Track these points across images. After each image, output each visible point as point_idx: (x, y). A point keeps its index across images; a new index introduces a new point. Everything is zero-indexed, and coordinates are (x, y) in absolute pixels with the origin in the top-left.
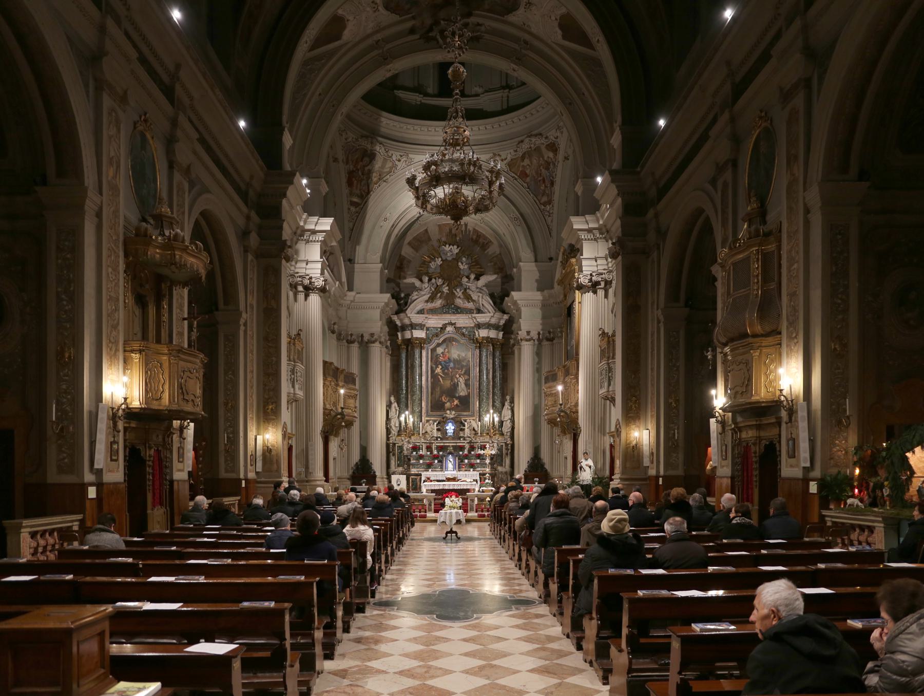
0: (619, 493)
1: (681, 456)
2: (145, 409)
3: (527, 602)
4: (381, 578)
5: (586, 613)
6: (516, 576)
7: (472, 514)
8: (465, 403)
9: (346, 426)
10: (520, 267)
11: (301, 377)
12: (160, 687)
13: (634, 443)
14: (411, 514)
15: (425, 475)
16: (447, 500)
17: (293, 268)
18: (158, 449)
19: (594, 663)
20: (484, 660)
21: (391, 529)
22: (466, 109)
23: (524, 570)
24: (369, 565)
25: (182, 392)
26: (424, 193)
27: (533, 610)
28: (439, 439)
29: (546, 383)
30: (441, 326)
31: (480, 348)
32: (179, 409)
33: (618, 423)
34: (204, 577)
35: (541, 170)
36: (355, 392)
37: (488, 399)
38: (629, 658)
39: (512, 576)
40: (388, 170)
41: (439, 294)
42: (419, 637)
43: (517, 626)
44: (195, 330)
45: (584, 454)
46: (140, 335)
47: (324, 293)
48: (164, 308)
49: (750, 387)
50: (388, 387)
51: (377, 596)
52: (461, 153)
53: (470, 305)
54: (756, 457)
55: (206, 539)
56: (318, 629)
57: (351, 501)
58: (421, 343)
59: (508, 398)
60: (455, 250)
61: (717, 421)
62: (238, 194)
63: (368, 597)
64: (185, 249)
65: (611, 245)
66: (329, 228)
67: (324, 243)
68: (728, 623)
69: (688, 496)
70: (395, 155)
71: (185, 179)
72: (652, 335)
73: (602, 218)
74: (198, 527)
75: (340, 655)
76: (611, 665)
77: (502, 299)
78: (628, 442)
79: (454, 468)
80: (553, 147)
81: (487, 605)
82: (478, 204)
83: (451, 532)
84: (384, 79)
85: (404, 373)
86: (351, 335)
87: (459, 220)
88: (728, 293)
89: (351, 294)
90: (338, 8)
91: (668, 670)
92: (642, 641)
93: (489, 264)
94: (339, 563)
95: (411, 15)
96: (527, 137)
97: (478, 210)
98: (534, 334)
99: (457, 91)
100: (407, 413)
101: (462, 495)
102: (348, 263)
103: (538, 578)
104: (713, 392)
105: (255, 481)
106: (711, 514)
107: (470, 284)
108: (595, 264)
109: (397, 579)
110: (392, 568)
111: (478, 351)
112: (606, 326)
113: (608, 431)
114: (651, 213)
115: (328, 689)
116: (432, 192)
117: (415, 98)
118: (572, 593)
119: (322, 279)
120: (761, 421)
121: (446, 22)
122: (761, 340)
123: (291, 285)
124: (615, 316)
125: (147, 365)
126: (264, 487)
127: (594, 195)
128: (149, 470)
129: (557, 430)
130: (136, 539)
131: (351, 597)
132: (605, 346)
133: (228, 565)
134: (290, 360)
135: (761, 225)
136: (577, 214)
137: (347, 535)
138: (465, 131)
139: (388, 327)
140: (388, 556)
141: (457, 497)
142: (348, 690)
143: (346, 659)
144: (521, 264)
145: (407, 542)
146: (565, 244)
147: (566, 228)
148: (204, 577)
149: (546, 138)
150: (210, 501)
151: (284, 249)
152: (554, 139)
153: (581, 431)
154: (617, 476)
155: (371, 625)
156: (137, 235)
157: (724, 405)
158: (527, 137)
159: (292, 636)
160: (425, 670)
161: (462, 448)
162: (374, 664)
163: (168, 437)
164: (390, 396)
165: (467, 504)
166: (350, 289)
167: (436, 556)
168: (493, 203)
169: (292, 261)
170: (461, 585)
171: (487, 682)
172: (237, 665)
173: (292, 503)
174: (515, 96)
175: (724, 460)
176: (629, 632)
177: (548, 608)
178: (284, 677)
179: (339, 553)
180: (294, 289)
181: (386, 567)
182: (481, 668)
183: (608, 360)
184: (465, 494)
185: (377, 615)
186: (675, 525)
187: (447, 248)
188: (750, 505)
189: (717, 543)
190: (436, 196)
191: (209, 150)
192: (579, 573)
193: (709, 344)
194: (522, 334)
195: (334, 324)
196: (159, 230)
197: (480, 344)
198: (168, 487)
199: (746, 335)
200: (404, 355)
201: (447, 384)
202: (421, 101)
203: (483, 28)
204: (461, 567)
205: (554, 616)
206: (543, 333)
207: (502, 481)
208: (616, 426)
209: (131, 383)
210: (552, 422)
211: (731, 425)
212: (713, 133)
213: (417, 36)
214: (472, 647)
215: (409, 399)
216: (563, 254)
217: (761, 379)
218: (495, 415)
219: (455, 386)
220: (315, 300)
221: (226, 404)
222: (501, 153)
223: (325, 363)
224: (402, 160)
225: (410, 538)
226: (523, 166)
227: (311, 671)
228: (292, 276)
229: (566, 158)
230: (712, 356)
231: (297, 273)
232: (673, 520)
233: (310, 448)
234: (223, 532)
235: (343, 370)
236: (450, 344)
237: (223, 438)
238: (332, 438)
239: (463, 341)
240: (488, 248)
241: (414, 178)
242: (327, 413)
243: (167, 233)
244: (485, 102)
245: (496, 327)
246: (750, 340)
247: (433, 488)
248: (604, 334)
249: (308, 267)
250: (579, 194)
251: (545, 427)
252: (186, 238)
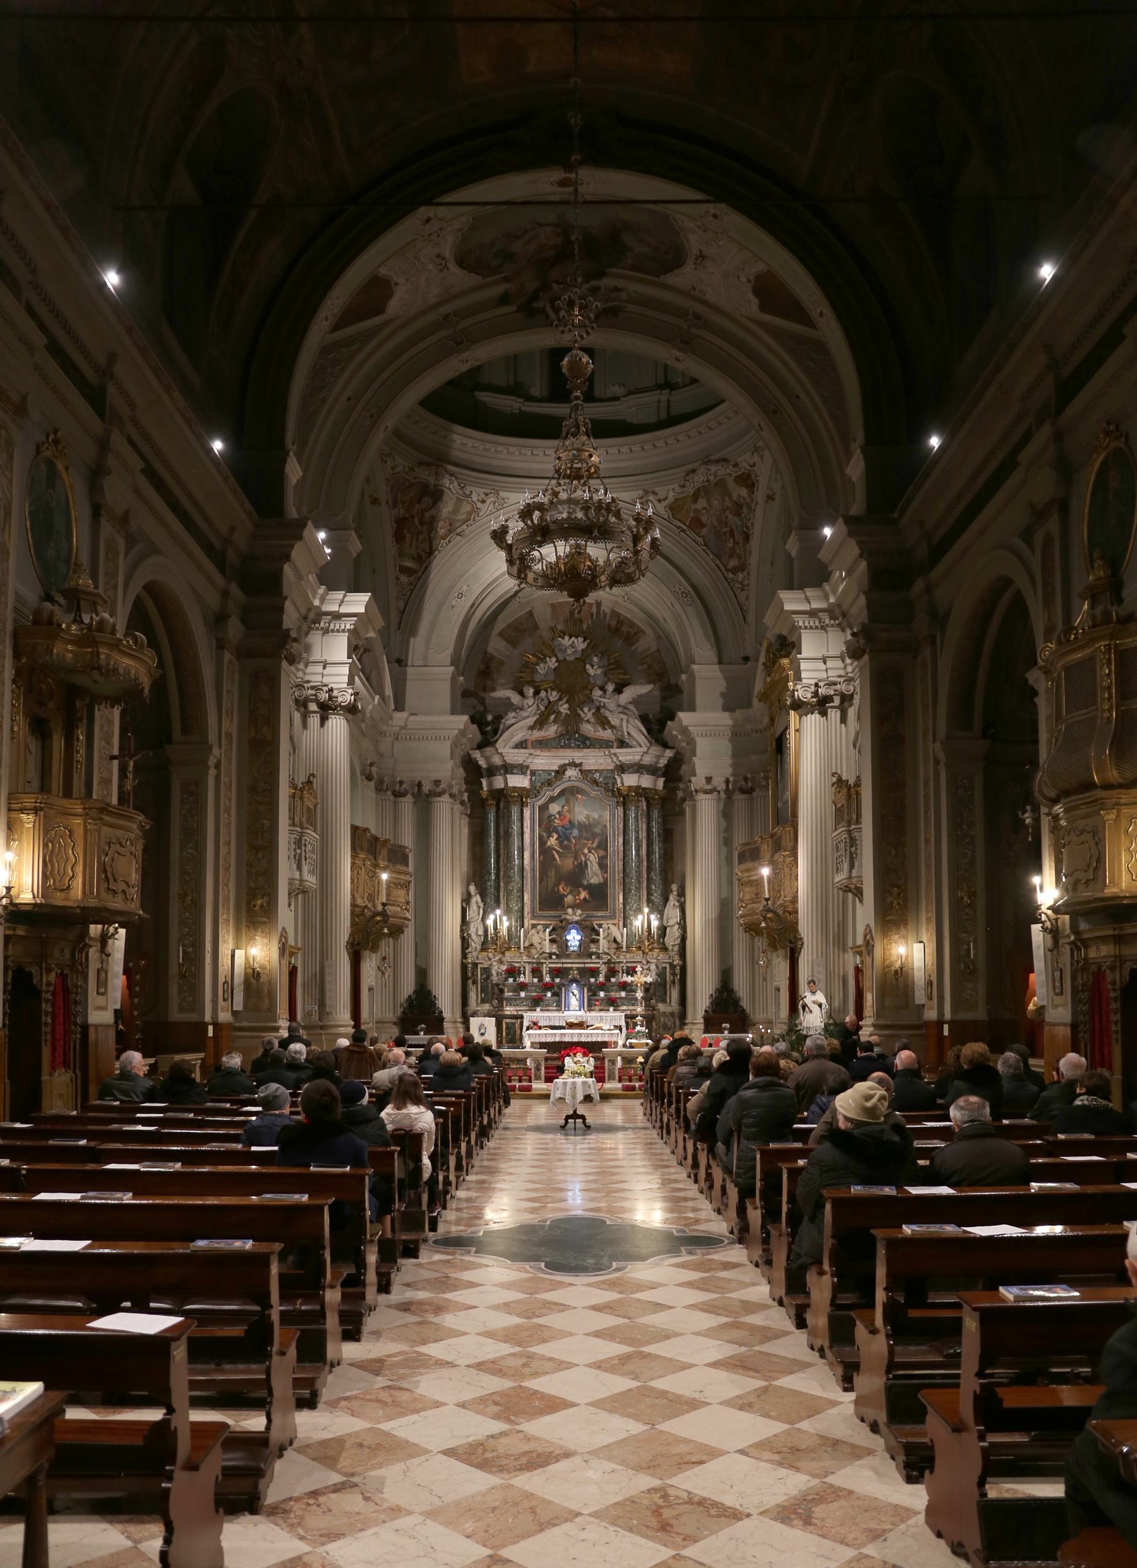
0: (873, 1051)
1: (981, 988)
2: (41, 905)
3: (708, 1242)
4: (448, 1197)
5: (812, 1264)
6: (689, 1194)
7: (612, 1086)
8: (599, 897)
9: (391, 934)
10: (693, 672)
11: (313, 852)
12: (42, 1389)
13: (898, 965)
14: (504, 1084)
15: (528, 1017)
16: (568, 1060)
17: (300, 674)
18: (62, 972)
19: (828, 1352)
20: (629, 1345)
21: (467, 1111)
22: (592, 421)
23: (702, 1183)
24: (426, 1175)
25: (106, 877)
26: (521, 554)
27: (719, 1256)
28: (554, 957)
29: (740, 863)
30: (556, 768)
31: (624, 804)
32: (99, 905)
33: (868, 931)
34: (131, 1194)
35: (727, 517)
36: (407, 878)
37: (639, 889)
38: (889, 1345)
39: (681, 1194)
40: (464, 516)
41: (553, 717)
42: (515, 1302)
43: (690, 1284)
44: (130, 776)
45: (809, 983)
46: (36, 784)
47: (353, 714)
48: (78, 739)
49: (1100, 872)
50: (465, 869)
51: (441, 1228)
52: (584, 491)
53: (607, 734)
54: (1114, 990)
55: (140, 1128)
56: (332, 1287)
57: (396, 1062)
58: (522, 796)
59: (674, 887)
60: (580, 644)
61: (1044, 929)
62: (209, 556)
63: (424, 1231)
64: (116, 645)
65: (849, 637)
66: (362, 610)
67: (354, 634)
68: (1064, 1286)
69: (993, 1057)
70: (477, 494)
71: (119, 532)
72: (926, 784)
73: (835, 594)
74: (127, 1105)
75: (372, 1333)
76: (859, 1356)
77: (662, 724)
78: (887, 962)
79: (581, 1006)
80: (747, 481)
81: (637, 1247)
82: (614, 572)
83: (575, 1116)
84: (458, 374)
85: (492, 846)
86: (401, 783)
87: (582, 597)
88: (1058, 716)
89: (400, 717)
90: (379, 266)
91: (958, 1366)
92: (913, 1313)
93: (639, 668)
94: (371, 1171)
95: (502, 275)
96: (700, 465)
97: (614, 582)
98: (719, 782)
99: (578, 393)
100: (498, 912)
101: (594, 1052)
102: (397, 665)
103: (727, 1198)
104: (1036, 880)
105: (231, 1027)
106: (1035, 1088)
107: (605, 700)
108: (823, 667)
109: (477, 1197)
110: (469, 1178)
111: (621, 809)
112: (844, 769)
113: (850, 944)
114: (919, 585)
115: (348, 1394)
116: (536, 553)
117: (510, 404)
118: (787, 1226)
119: (350, 691)
120: (1122, 929)
121: (561, 286)
122: (1120, 793)
123: (297, 701)
124: (859, 752)
125: (46, 832)
126: (251, 1037)
127: (819, 556)
128: (46, 1007)
129: (761, 943)
130: (18, 1125)
131: (393, 1230)
132: (843, 801)
133: (176, 1174)
134: (293, 825)
135: (1112, 605)
136: (790, 587)
137: (386, 1122)
138: (591, 456)
139: (465, 768)
140: (462, 1157)
141: (585, 1055)
142: (384, 1396)
143: (382, 1339)
144: (695, 667)
145: (496, 1134)
146: (771, 635)
147: (769, 612)
148: (131, 1194)
149: (736, 465)
150: (152, 1061)
151: (286, 643)
152: (748, 467)
153: (803, 943)
154: (868, 1022)
155: (428, 1281)
156: (36, 622)
157: (1056, 902)
158: (702, 464)
159: (283, 1298)
160: (524, 1360)
161: (594, 972)
162: (433, 1350)
163: (81, 952)
164: (468, 885)
165: (604, 1068)
166: (400, 706)
167: (548, 1159)
168: (641, 571)
169: (299, 663)
170: (592, 1210)
171: (634, 1384)
172: (179, 1352)
173: (294, 1066)
174: (681, 400)
175: (1057, 994)
176: (888, 1298)
177: (746, 1251)
178: (268, 1372)
179: (371, 1154)
180: (302, 709)
181: (458, 1177)
182: (625, 1359)
183: (849, 826)
184: (600, 1051)
185: (441, 1261)
186: (969, 1110)
187: (566, 641)
188: (1105, 1073)
189: (1048, 1141)
190: (542, 559)
191: (159, 485)
192: (798, 1192)
193: (1027, 799)
194: (698, 782)
195: (372, 764)
196: (73, 615)
197: (624, 798)
198: (78, 1036)
199: (1091, 786)
200: (492, 817)
201: (569, 863)
202: (520, 409)
203: (624, 296)
204: (591, 1178)
205: (757, 1265)
206: (735, 782)
207: (666, 1028)
208: (865, 936)
209: (20, 862)
210: (752, 929)
211: (1068, 936)
212: (1025, 457)
213: (513, 308)
214: (607, 1321)
215: (502, 889)
216: (768, 651)
217: (1120, 855)
218: (653, 917)
219: (582, 868)
220: (337, 725)
221: (183, 897)
222: (657, 490)
223: (355, 829)
224: (488, 501)
225: (501, 1125)
226: (696, 510)
227: (318, 1362)
228: (300, 686)
229: (770, 498)
230: (1033, 819)
231: (308, 682)
232: (966, 1101)
233: (327, 970)
234: (170, 1114)
235: (387, 841)
236: (572, 799)
237: (177, 954)
238: (366, 954)
239: (594, 792)
240: (638, 641)
241: (504, 530)
242: (357, 912)
243: (86, 619)
244: (629, 409)
245: (652, 770)
246: (1099, 793)
247: (543, 1040)
248: (840, 783)
249: (325, 672)
250: (793, 554)
251: (740, 938)
252: (117, 628)
